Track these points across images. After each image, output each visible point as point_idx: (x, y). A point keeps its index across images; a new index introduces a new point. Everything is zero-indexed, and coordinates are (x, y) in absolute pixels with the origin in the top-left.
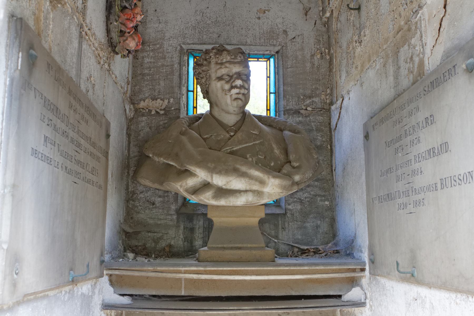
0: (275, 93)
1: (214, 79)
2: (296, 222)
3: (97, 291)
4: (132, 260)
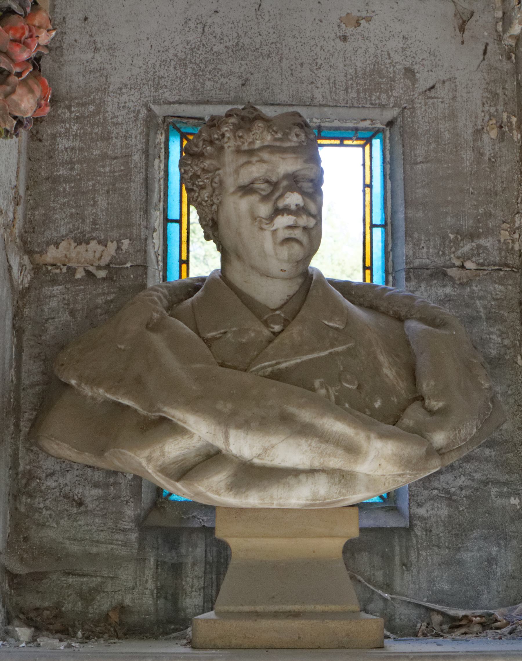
1: (232, 190)
2: (436, 549)
4: (27, 643)
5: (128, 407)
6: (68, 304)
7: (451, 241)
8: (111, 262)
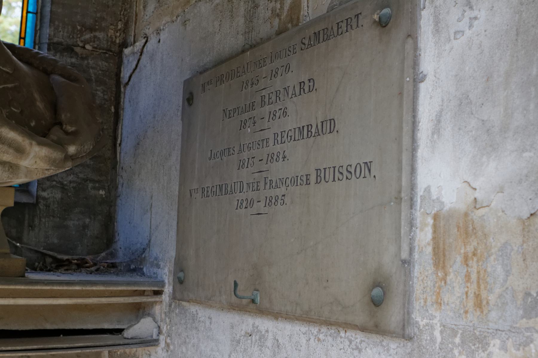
0: (36, 13)
2: (52, 218)
7: (78, 31)
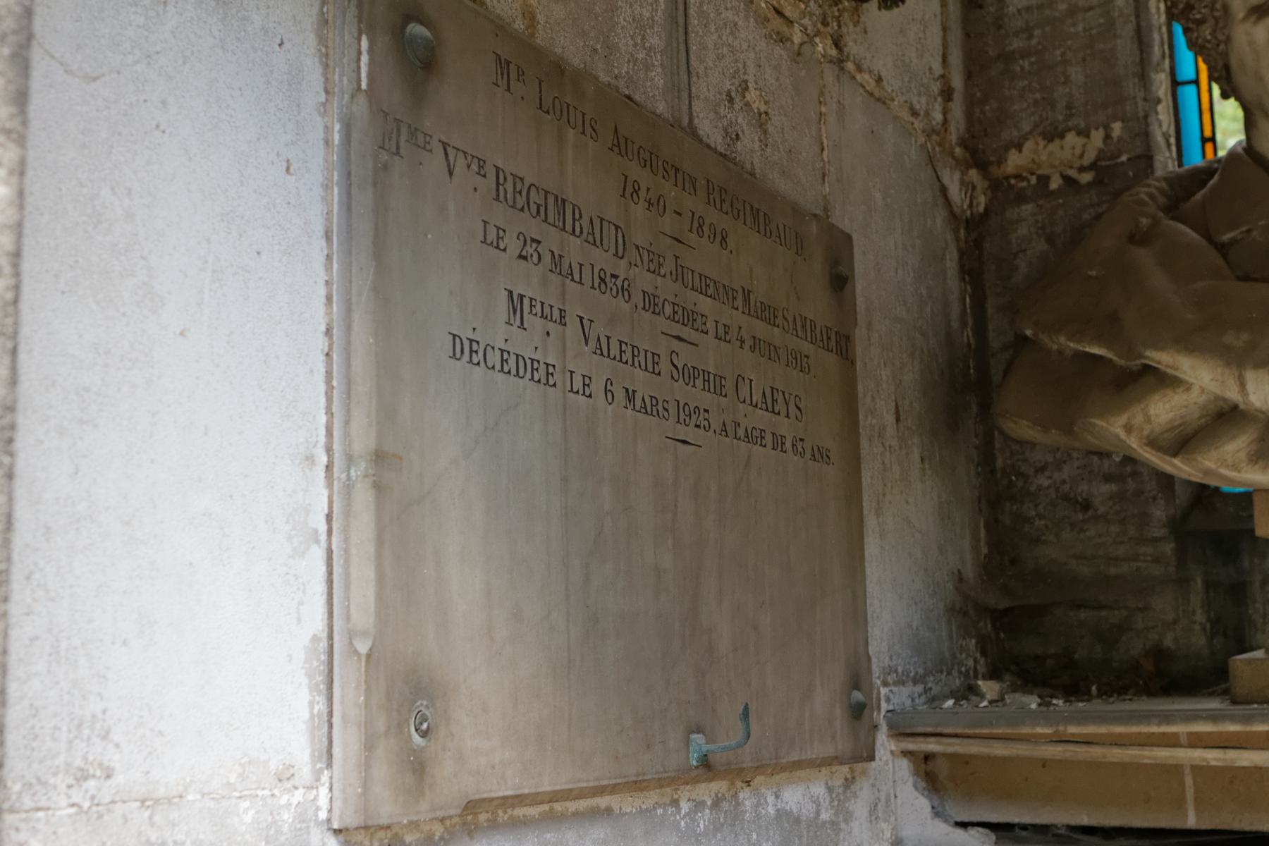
1: (1241, 15)
3: (859, 808)
4: (991, 702)
5: (1101, 357)
6: (1042, 228)
8: (1098, 159)
